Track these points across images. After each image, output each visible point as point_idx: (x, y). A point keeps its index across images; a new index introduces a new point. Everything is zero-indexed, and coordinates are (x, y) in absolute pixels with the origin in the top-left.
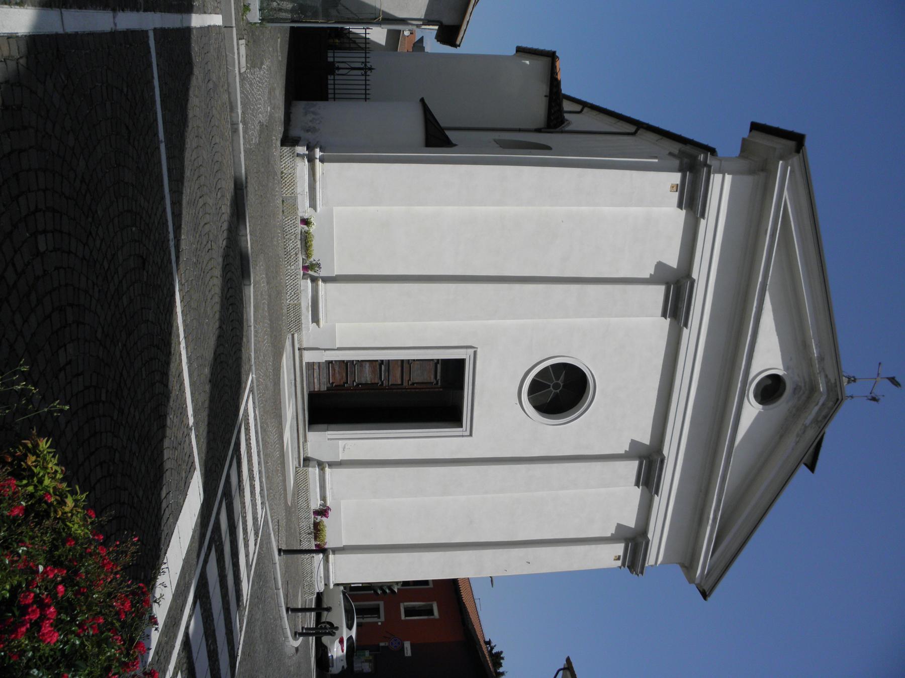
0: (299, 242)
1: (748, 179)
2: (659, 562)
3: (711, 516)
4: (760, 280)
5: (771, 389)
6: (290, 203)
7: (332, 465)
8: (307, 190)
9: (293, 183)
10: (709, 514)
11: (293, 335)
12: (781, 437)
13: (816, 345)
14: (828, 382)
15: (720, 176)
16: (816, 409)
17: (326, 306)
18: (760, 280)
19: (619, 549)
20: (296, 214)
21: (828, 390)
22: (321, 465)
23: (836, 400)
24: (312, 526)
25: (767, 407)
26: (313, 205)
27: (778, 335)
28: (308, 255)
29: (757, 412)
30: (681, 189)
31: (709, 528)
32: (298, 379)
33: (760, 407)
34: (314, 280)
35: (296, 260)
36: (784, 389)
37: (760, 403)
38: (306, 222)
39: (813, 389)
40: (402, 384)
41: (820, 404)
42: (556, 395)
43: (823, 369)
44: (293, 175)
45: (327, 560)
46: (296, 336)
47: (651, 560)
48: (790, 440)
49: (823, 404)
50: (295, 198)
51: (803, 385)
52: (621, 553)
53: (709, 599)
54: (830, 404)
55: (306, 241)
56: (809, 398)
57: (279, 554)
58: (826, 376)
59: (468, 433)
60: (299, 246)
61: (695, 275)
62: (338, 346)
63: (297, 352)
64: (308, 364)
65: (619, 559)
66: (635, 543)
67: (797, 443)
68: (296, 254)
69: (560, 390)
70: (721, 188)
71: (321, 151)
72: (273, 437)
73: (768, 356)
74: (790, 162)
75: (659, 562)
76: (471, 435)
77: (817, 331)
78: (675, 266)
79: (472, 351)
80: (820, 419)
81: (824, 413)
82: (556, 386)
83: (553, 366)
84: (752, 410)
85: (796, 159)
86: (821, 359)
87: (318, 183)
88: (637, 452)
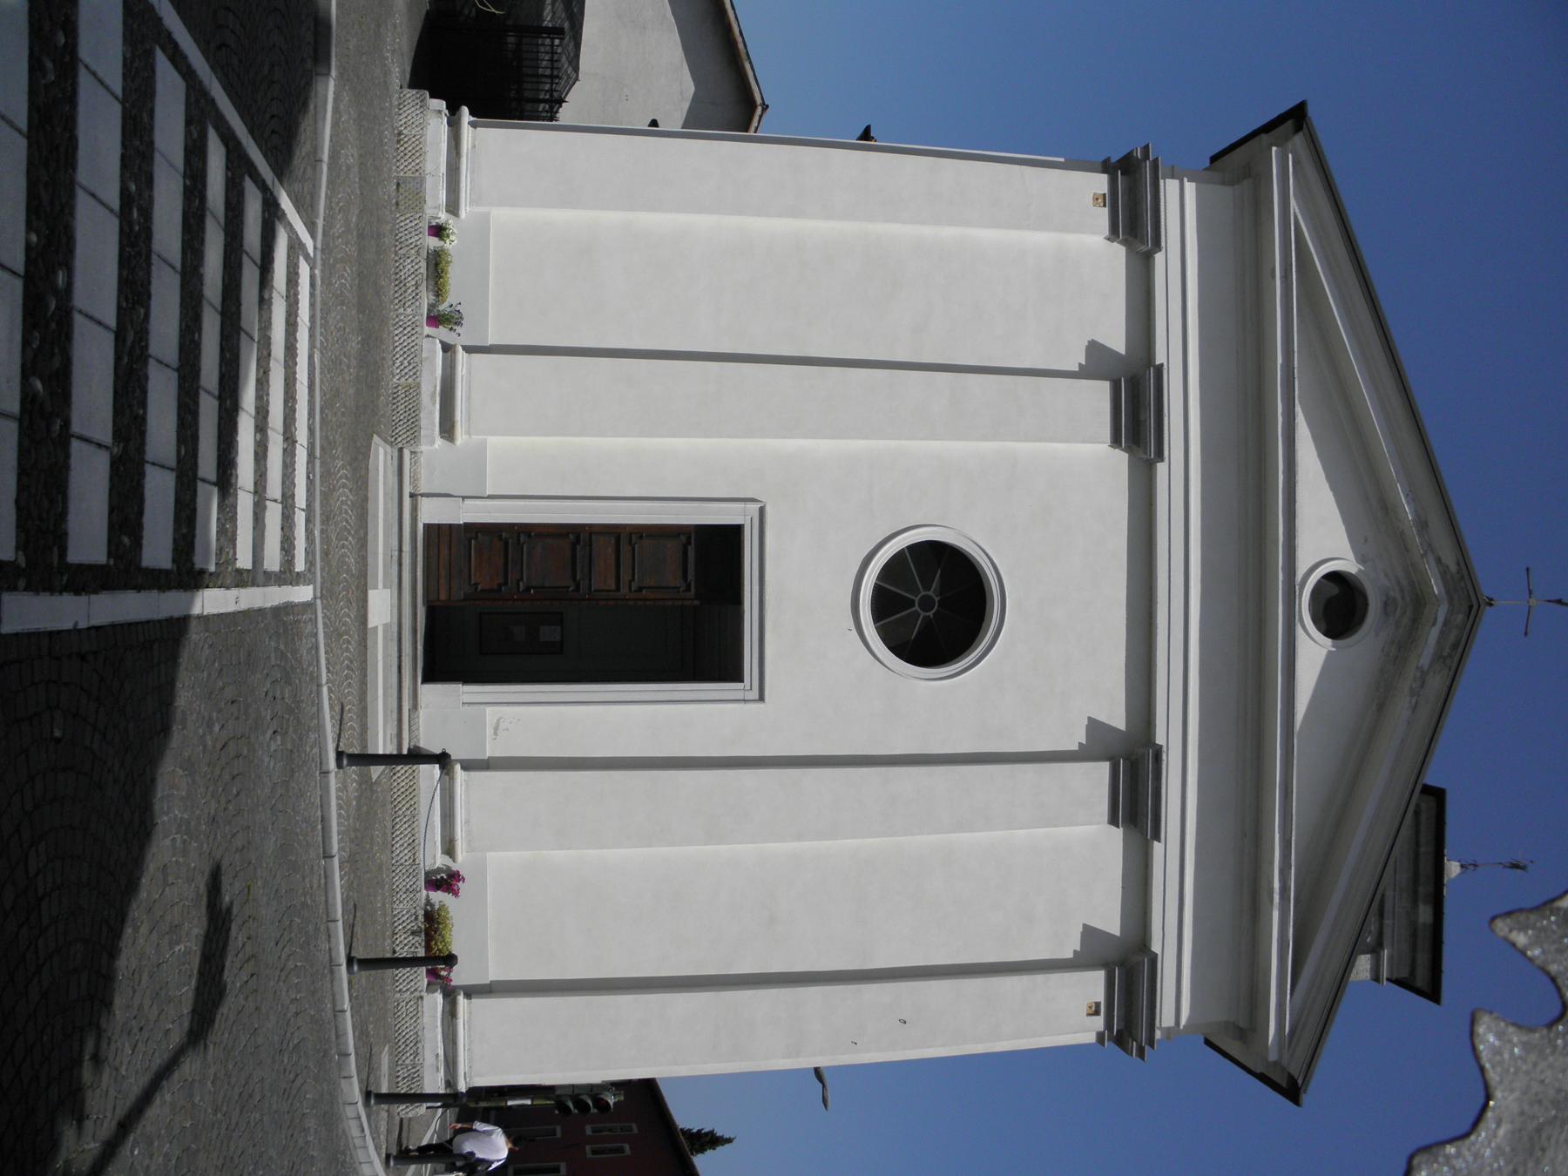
0: (423, 264)
1: (1226, 193)
2: (1183, 1021)
3: (1276, 885)
4: (1280, 360)
5: (1340, 606)
6: (411, 191)
7: (468, 766)
8: (443, 169)
9: (419, 152)
10: (1271, 882)
11: (401, 450)
12: (1381, 707)
13: (1407, 496)
14: (1444, 573)
15: (1176, 182)
16: (1434, 633)
17: (469, 398)
18: (1280, 360)
19: (1093, 985)
20: (422, 209)
21: (1447, 592)
22: (443, 759)
23: (1470, 603)
24: (421, 918)
25: (1340, 642)
26: (453, 207)
27: (1332, 489)
28: (439, 293)
29: (1324, 652)
30: (1111, 200)
31: (1276, 914)
32: (407, 547)
33: (1328, 641)
34: (450, 994)
35: (416, 297)
36: (1366, 604)
37: (1327, 634)
38: (438, 231)
39: (1419, 601)
40: (618, 589)
41: (1440, 620)
42: (928, 623)
43: (1430, 547)
44: (419, 141)
45: (451, 1013)
46: (406, 453)
47: (1166, 1018)
48: (1401, 707)
49: (1446, 623)
50: (422, 181)
51: (1398, 596)
52: (1100, 996)
53: (1305, 1098)
54: (1460, 618)
55: (436, 265)
56: (1415, 620)
57: (339, 765)
58: (1439, 561)
59: (755, 694)
60: (423, 270)
61: (1156, 947)
62: (488, 493)
63: (407, 501)
64: (428, 527)
65: (1097, 1013)
66: (1127, 967)
67: (1414, 708)
68: (417, 286)
69: (934, 605)
70: (1181, 204)
71: (472, 113)
72: (344, 496)
73: (1323, 538)
74: (1290, 146)
75: (1183, 1021)
76: (761, 698)
77: (1411, 477)
78: (1122, 351)
79: (755, 507)
80: (1447, 651)
81: (1452, 638)
82: (926, 604)
83: (914, 548)
84: (1314, 650)
85: (1299, 140)
86: (1422, 525)
87: (464, 160)
88: (1099, 744)
